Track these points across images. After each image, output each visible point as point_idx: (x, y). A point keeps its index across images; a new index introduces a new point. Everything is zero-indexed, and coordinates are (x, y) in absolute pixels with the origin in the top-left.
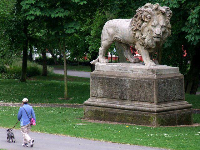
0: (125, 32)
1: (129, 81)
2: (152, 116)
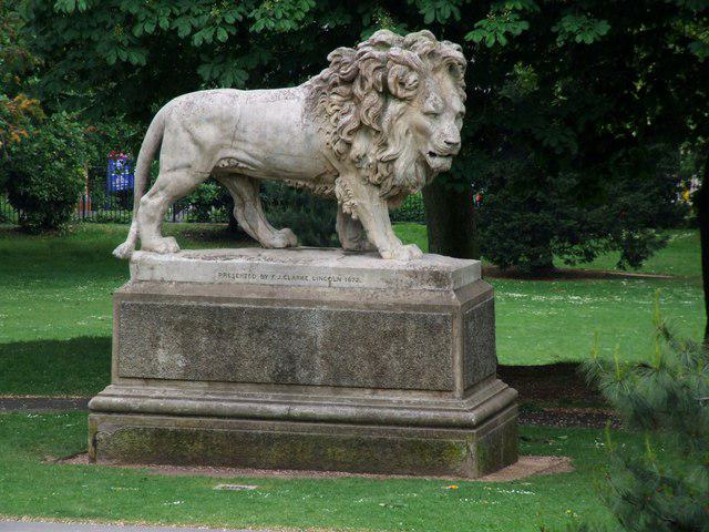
0: (285, 138)
2: (453, 441)
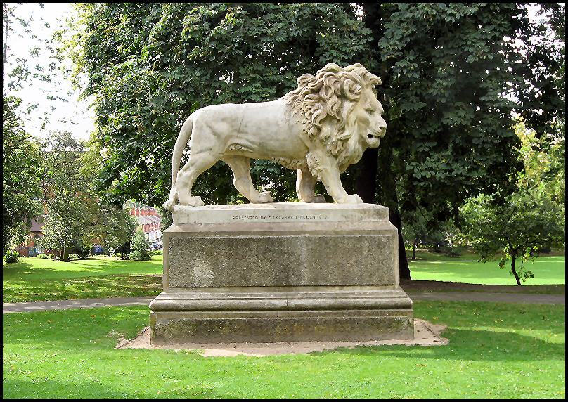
1: (310, 240)
